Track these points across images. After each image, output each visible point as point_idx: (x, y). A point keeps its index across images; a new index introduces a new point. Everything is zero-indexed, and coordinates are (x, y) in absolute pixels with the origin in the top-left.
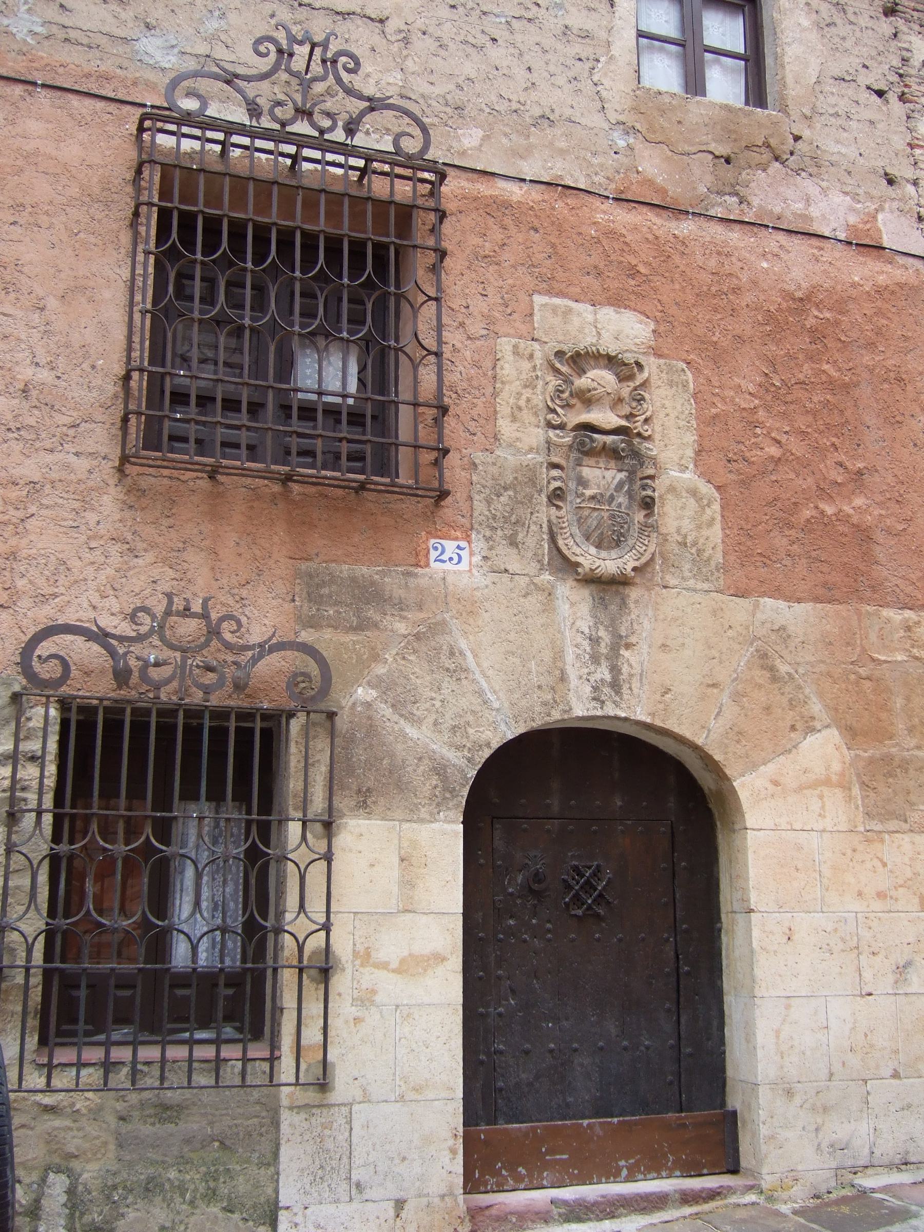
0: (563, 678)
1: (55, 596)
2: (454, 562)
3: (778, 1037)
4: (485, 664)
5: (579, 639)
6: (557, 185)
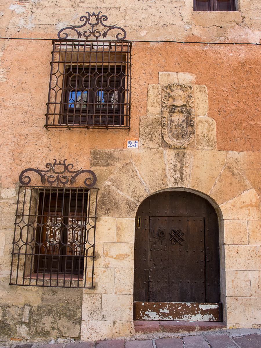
0: (165, 177)
1: (31, 162)
3: (233, 282)
4: (142, 174)
5: (171, 165)
6: (168, 42)
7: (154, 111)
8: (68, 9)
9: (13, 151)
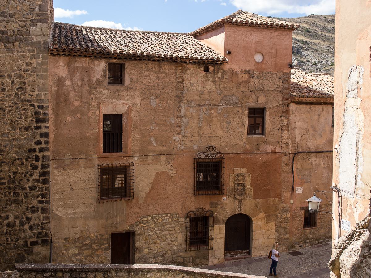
0: (235, 210)
2: (225, 199)
7: (232, 185)
8: (197, 138)
9: (182, 204)
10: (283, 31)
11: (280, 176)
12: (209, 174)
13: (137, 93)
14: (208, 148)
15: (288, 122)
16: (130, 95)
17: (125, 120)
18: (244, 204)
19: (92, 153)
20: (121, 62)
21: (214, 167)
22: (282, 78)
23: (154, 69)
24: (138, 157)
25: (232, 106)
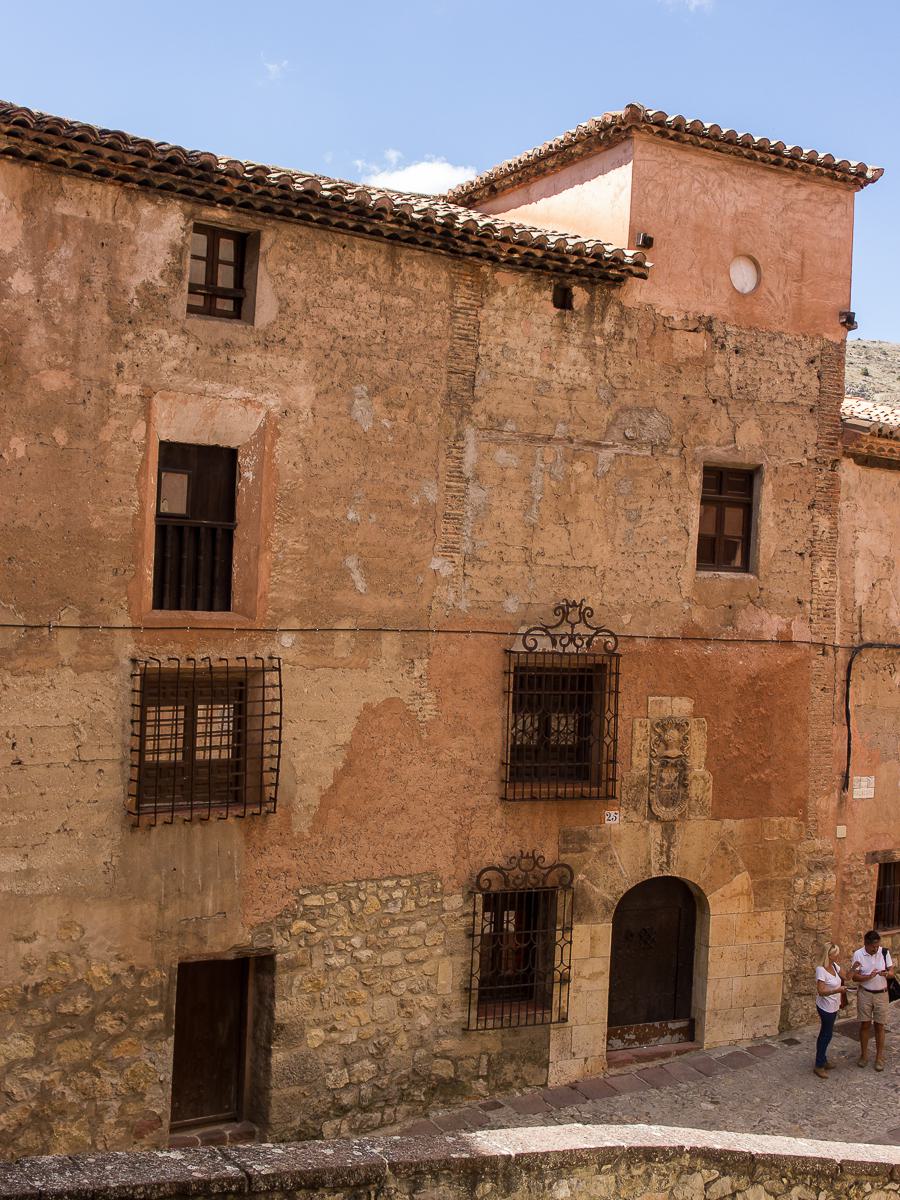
2: (614, 818)
8: (519, 569)
10: (825, 185)
11: (806, 731)
12: (559, 715)
13: (303, 363)
14: (563, 610)
15: (834, 529)
16: (272, 370)
17: (249, 475)
18: (680, 837)
19: (111, 607)
20: (247, 223)
21: (564, 688)
22: (818, 363)
23: (371, 272)
24: (294, 636)
25: (648, 453)
